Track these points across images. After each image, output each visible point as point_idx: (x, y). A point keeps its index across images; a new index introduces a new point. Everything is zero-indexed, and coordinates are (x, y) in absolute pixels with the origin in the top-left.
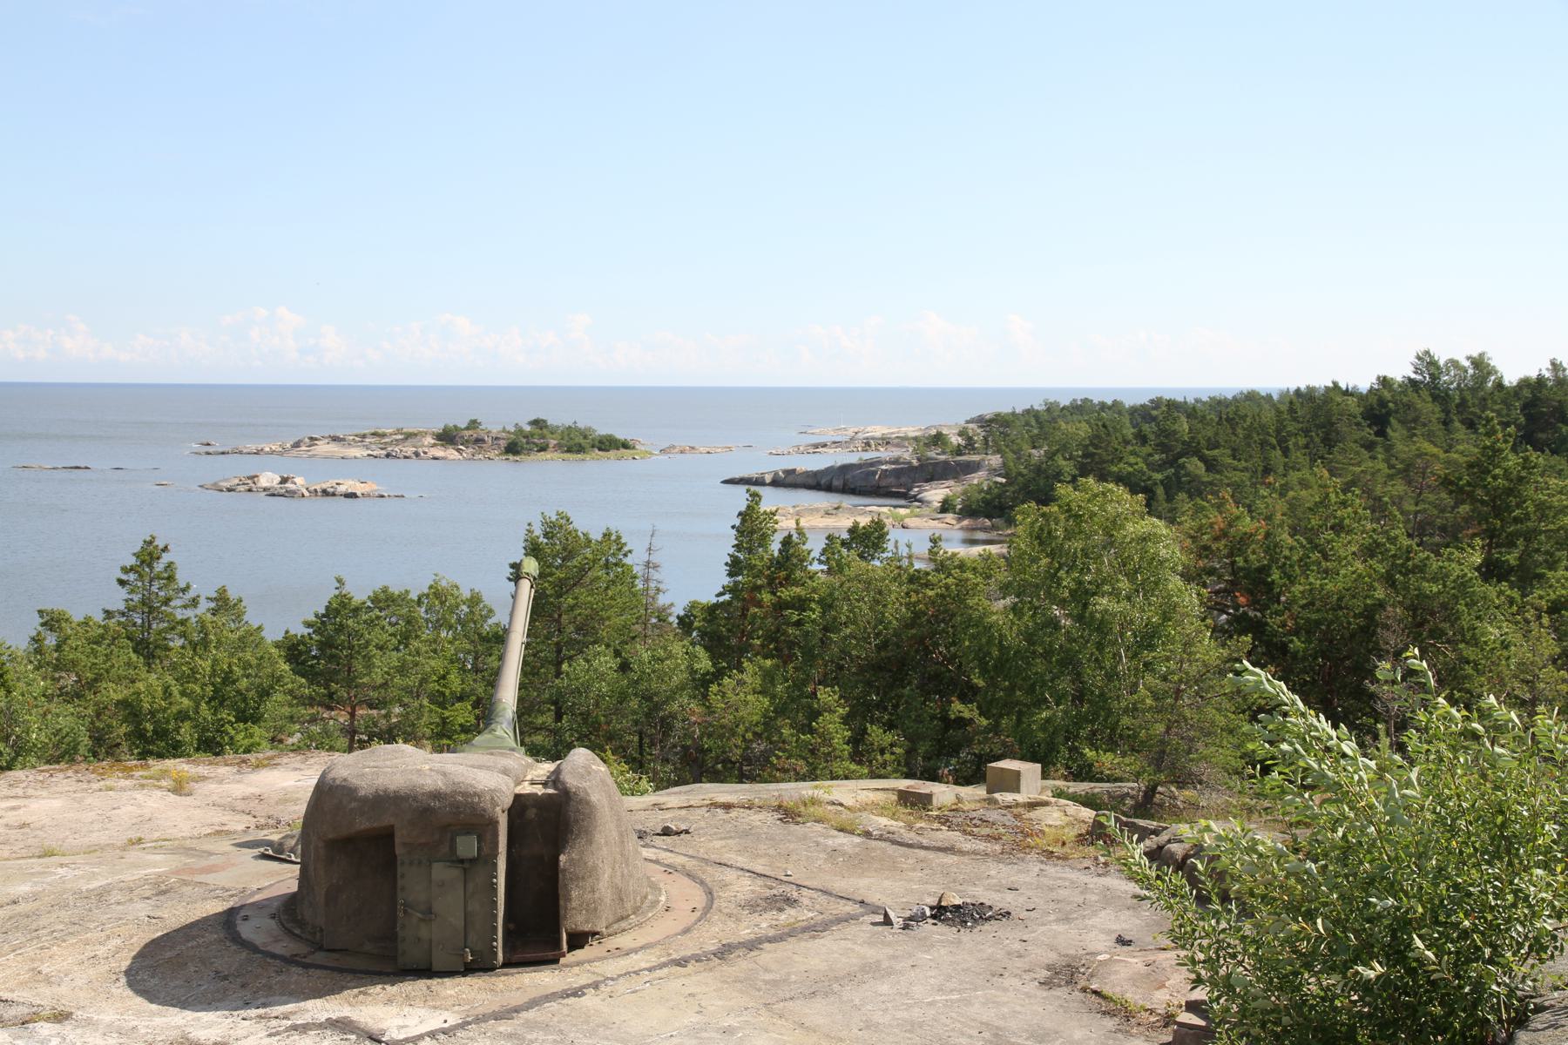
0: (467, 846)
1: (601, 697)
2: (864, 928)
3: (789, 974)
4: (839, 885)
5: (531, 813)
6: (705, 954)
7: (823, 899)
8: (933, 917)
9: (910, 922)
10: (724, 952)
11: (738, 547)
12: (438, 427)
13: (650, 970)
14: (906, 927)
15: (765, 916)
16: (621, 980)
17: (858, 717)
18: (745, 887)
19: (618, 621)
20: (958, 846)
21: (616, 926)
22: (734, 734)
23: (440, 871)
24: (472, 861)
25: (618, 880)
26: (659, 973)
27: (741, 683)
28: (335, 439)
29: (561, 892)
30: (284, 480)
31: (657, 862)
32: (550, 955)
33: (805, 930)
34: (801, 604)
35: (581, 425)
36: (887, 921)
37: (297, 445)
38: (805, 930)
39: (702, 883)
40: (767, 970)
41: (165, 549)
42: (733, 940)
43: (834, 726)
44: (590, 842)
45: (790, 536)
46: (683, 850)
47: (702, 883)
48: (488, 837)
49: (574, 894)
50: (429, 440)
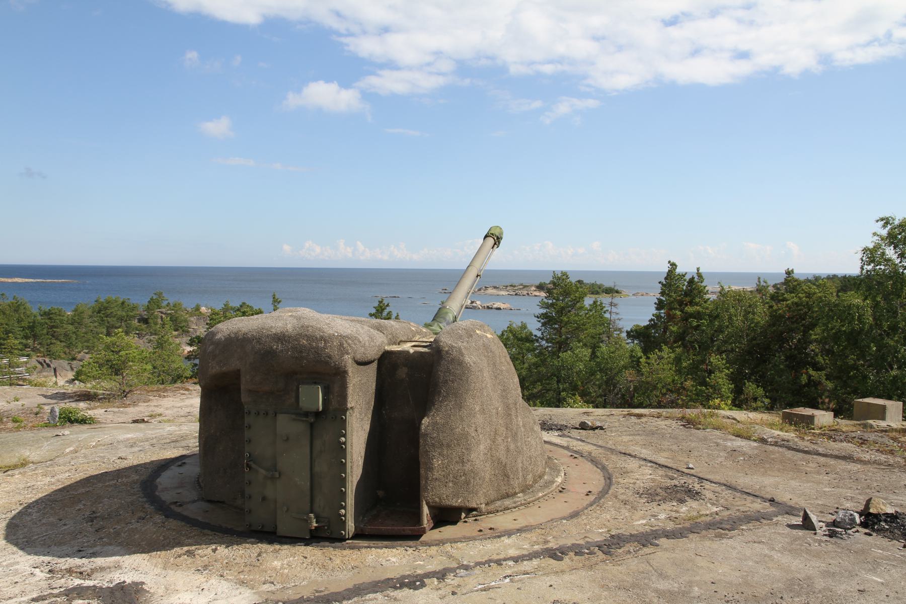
0: (315, 398)
1: (581, 371)
2: (779, 531)
3: (690, 584)
4: (744, 481)
5: (402, 373)
6: (589, 545)
7: (727, 493)
8: (864, 525)
9: (836, 529)
10: (611, 545)
11: (662, 294)
12: (537, 283)
13: (516, 560)
14: (832, 534)
15: (664, 506)
16: (477, 570)
17: (737, 381)
18: (645, 476)
19: (592, 331)
20: (856, 455)
21: (498, 503)
22: (655, 388)
23: (286, 424)
24: (317, 414)
25: (501, 453)
26: (527, 565)
27: (661, 358)
28: (495, 287)
29: (422, 460)
30: (472, 302)
31: (567, 448)
32: (408, 529)
33: (709, 526)
34: (698, 316)
35: (598, 283)
36: (807, 524)
37: (480, 290)
38: (709, 526)
39: (604, 468)
40: (662, 576)
41: (388, 305)
42: (625, 531)
43: (721, 379)
44: (460, 407)
45: (693, 278)
46: (594, 441)
47: (604, 468)
48: (336, 388)
49: (437, 463)
50: (533, 288)
